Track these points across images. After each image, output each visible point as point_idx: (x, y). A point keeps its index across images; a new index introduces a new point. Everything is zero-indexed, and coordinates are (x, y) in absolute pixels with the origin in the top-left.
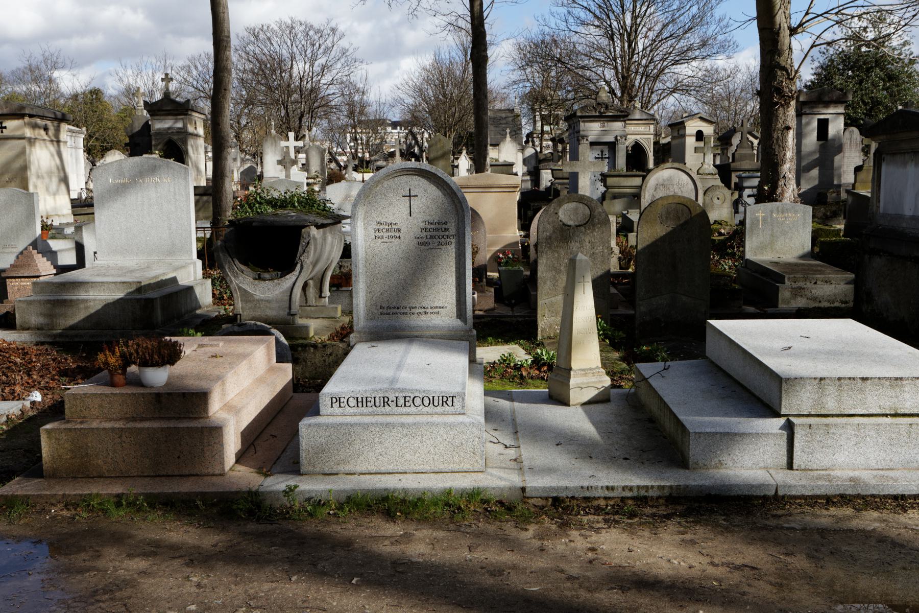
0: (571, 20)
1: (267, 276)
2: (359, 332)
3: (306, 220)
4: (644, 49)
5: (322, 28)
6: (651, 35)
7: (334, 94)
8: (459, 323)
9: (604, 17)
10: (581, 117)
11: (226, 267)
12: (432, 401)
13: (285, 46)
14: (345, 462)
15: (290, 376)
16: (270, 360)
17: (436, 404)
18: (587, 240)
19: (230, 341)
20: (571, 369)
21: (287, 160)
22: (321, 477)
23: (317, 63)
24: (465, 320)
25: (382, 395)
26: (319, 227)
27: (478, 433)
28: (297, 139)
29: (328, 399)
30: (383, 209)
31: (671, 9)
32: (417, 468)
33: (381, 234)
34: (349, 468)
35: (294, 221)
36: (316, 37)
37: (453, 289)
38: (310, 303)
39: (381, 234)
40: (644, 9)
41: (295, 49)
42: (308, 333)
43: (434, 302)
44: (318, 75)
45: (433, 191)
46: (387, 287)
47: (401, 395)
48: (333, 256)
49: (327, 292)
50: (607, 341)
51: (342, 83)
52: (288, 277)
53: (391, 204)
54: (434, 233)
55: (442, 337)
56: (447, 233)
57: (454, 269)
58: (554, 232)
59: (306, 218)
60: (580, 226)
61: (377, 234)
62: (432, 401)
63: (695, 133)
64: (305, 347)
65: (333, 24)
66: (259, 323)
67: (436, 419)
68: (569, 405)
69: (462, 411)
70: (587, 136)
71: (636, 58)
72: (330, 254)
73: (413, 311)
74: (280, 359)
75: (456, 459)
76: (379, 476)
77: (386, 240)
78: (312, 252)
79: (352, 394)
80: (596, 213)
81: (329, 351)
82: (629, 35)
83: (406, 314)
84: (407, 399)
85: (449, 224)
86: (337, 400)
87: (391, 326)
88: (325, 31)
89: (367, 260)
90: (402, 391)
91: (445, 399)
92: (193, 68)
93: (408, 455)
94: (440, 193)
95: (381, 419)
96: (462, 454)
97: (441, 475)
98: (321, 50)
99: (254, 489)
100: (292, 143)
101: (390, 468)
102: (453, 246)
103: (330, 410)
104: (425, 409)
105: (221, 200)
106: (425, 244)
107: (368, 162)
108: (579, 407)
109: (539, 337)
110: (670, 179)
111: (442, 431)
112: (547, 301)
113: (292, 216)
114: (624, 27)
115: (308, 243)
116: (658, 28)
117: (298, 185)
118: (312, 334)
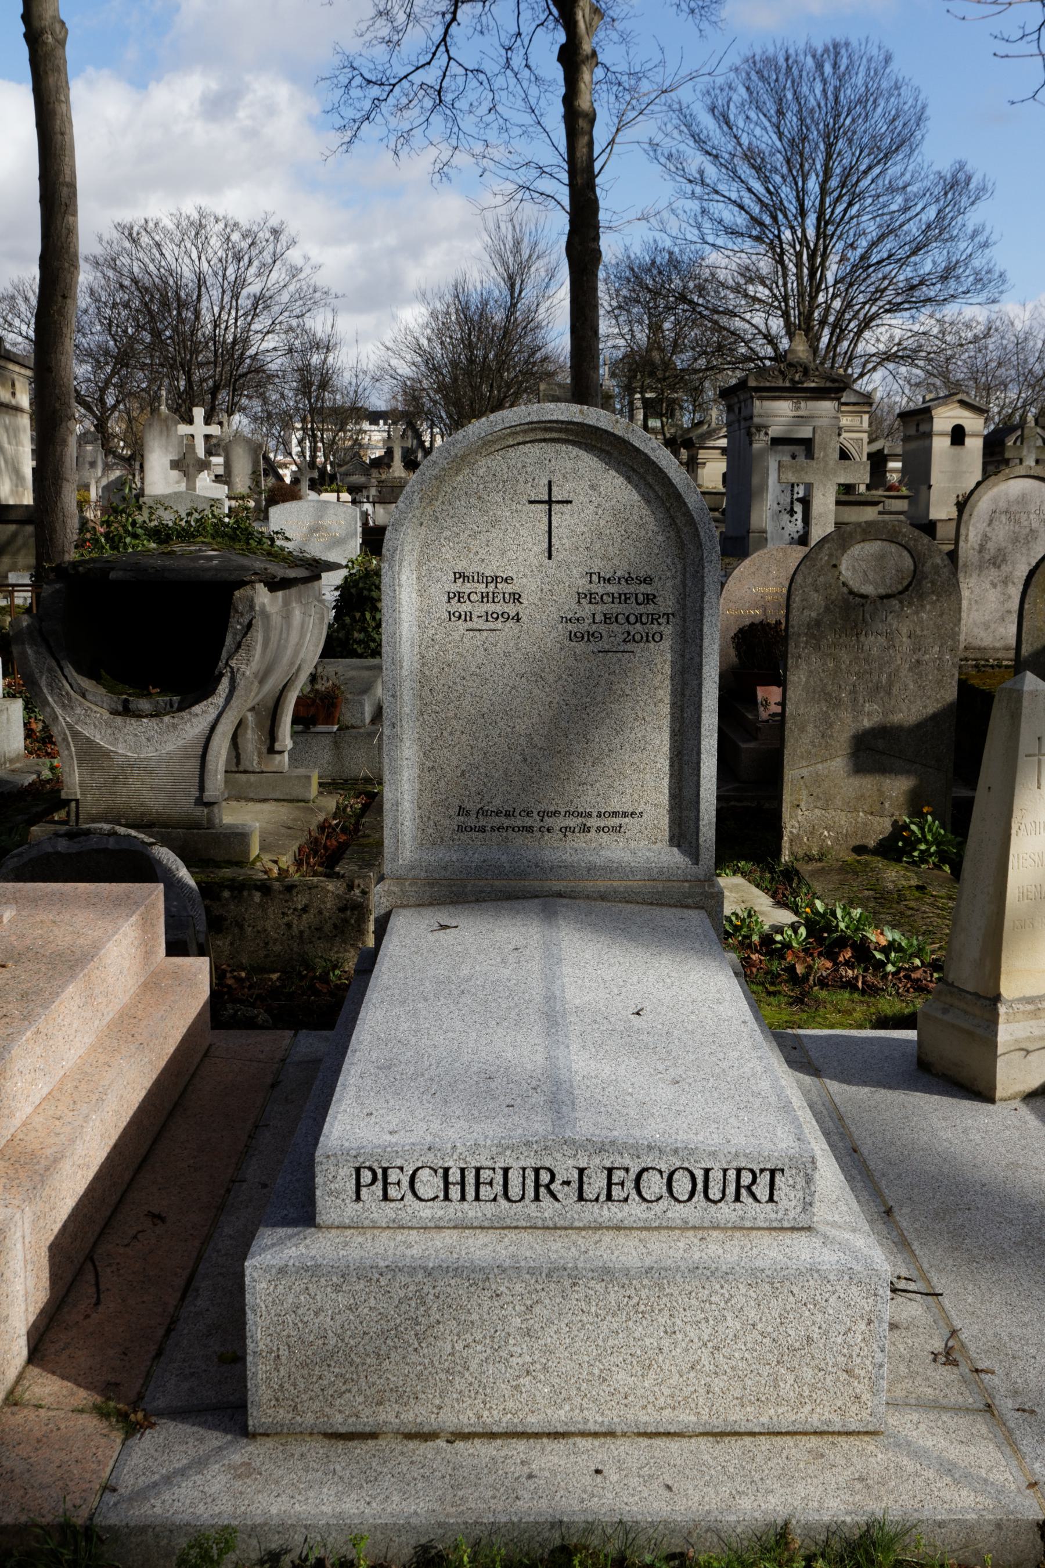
0: (707, 225)
1: (144, 705)
2: (399, 879)
3: (244, 569)
4: (836, 282)
5: (255, 228)
6: (854, 256)
7: (275, 349)
8: (674, 858)
9: (768, 220)
10: (757, 389)
11: (43, 683)
12: (701, 1186)
13: (187, 261)
14: (402, 1398)
15: (204, 992)
16: (148, 954)
17: (715, 1193)
18: (904, 631)
19: (35, 901)
20: (997, 998)
21: (190, 460)
22: (318, 1448)
23: (244, 293)
24: (693, 852)
25: (531, 1162)
26: (275, 585)
27: (867, 1304)
28: (207, 422)
29: (346, 1172)
30: (474, 535)
31: (886, 210)
32: (648, 1419)
33: (466, 607)
34: (418, 1414)
35: (216, 569)
36: (244, 245)
37: (664, 764)
38: (245, 764)
39: (466, 607)
40: (840, 209)
41: (205, 265)
42: (246, 852)
43: (607, 798)
44: (245, 314)
45: (615, 489)
46: (478, 757)
47: (595, 1164)
48: (302, 655)
49: (286, 739)
50: (947, 868)
51: (291, 329)
52: (197, 709)
53: (495, 523)
54: (616, 608)
55: (628, 898)
56: (650, 608)
57: (666, 709)
58: (827, 609)
59: (246, 562)
60: (888, 596)
61: (455, 606)
62: (701, 1186)
63: (949, 429)
64: (240, 888)
65: (274, 222)
66: (122, 830)
67: (718, 1250)
68: (991, 1100)
69: (803, 1221)
70: (767, 427)
71: (821, 298)
72: (296, 653)
73: (549, 821)
74: (175, 948)
76: (521, 1445)
77: (480, 624)
78: (259, 648)
79: (430, 1158)
80: (928, 568)
81: (301, 901)
82: (812, 257)
83: (530, 829)
85: (657, 584)
86: (375, 1176)
87: (505, 868)
88: (261, 235)
89: (423, 680)
90: (601, 1149)
91: (746, 1179)
92: (20, 301)
93: (621, 1377)
94: (636, 497)
95: (529, 1248)
96: (808, 1374)
97: (736, 1445)
98: (253, 270)
99: (79, 1519)
100: (199, 428)
101: (559, 1417)
102: (666, 644)
103: (352, 1209)
104: (678, 1212)
105: (53, 530)
106: (590, 636)
107: (333, 478)
108: (1016, 1103)
109: (786, 857)
110: (1023, 499)
111: (742, 1294)
112: (805, 772)
113: (211, 558)
114: (804, 241)
115: (250, 625)
116: (864, 243)
117: (214, 502)
118: (255, 851)
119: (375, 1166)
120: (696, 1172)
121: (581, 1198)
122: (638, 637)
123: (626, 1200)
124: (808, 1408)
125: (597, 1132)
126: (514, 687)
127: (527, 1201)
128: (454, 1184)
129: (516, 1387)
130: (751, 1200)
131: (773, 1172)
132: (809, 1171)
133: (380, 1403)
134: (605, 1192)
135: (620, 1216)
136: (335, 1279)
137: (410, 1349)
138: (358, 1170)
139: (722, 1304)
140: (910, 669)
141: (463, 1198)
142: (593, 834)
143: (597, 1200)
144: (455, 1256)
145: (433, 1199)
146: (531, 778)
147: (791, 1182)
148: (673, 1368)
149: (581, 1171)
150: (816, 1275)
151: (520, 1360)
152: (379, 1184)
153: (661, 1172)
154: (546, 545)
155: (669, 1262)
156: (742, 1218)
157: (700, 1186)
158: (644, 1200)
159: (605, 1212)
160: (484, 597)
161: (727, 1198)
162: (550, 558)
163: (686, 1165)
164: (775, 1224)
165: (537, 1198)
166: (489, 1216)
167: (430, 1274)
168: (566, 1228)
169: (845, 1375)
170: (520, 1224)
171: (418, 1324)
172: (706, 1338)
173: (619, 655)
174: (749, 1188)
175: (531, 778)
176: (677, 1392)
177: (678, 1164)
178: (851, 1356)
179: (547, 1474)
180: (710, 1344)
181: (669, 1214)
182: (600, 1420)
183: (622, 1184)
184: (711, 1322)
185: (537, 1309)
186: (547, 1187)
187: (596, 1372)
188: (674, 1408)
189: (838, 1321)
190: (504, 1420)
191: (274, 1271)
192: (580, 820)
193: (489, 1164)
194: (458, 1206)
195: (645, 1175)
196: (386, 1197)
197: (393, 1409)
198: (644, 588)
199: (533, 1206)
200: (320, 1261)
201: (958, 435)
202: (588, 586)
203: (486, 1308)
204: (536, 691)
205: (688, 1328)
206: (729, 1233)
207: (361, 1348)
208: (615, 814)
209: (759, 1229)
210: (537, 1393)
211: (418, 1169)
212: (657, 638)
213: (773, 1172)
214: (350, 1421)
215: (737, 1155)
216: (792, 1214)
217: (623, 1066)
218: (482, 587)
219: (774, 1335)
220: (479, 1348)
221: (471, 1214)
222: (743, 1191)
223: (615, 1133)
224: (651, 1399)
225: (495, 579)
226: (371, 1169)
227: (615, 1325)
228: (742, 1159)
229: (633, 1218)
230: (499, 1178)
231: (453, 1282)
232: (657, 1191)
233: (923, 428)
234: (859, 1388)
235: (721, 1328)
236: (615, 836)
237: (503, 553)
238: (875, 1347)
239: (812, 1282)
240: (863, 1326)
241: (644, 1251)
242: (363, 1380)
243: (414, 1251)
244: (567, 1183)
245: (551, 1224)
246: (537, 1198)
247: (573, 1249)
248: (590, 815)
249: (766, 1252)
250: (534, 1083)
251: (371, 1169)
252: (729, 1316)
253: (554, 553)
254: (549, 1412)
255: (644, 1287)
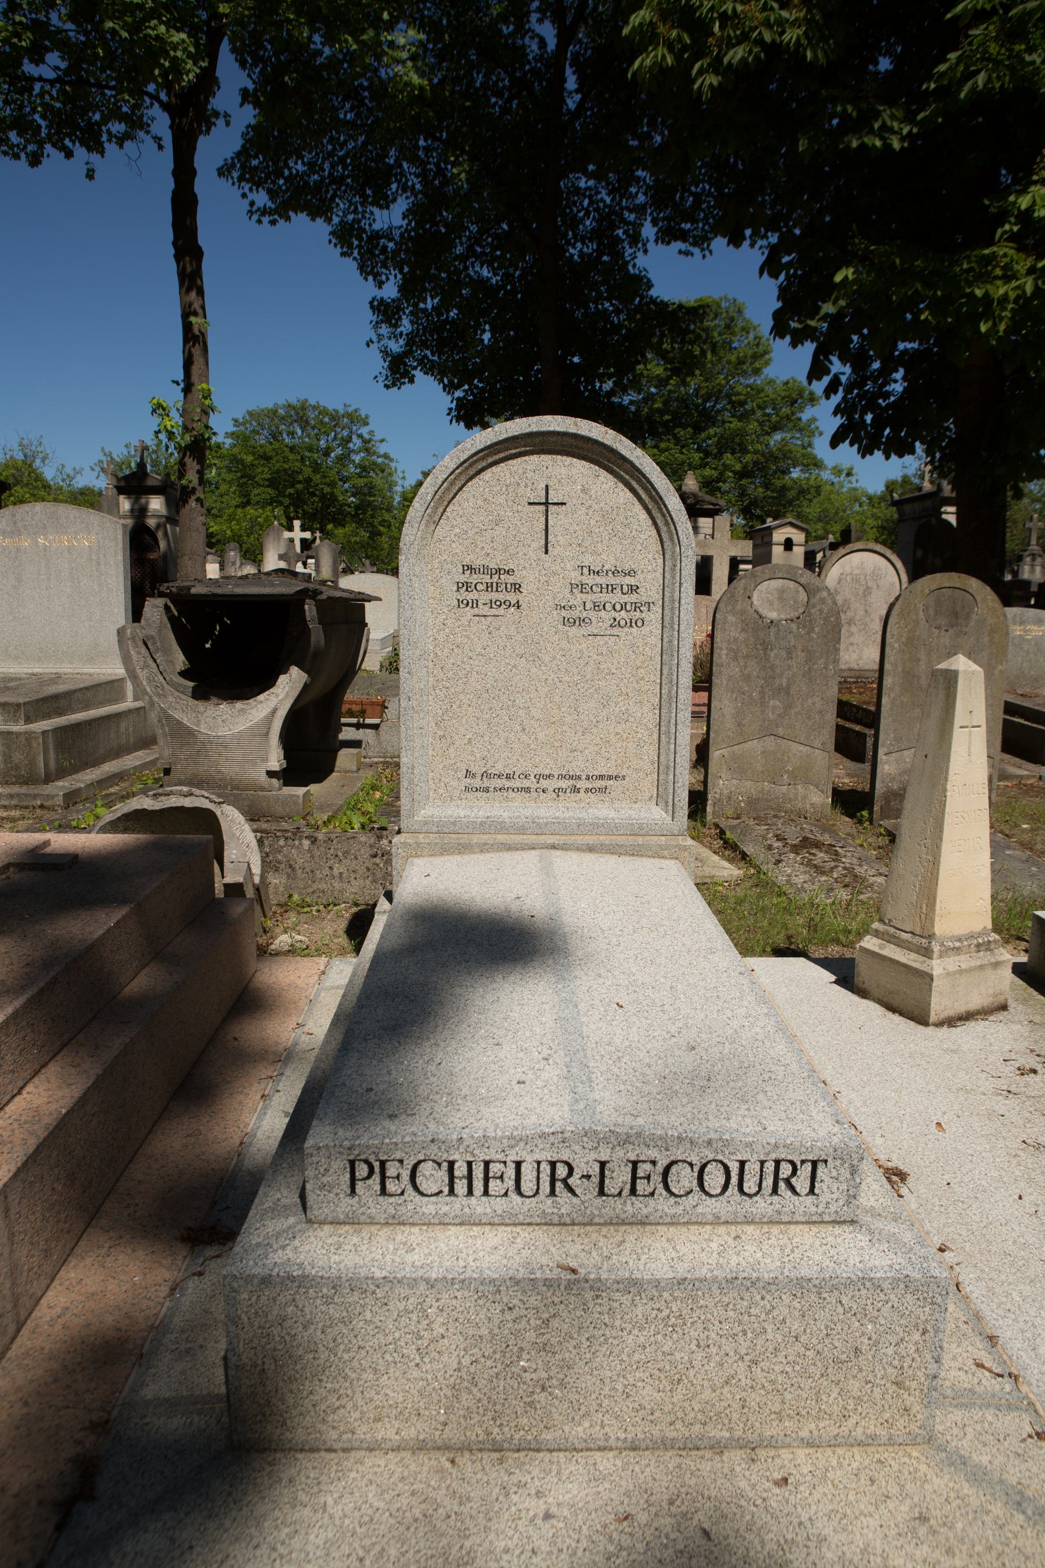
12: (735, 1179)
17: (750, 1186)
28: (303, 529)
39: (471, 596)
56: (634, 598)
61: (464, 595)
69: (846, 1213)
75: (832, 1401)
77: (484, 610)
79: (433, 1151)
84: (643, 1169)
85: (640, 576)
90: (625, 1141)
91: (786, 1170)
96: (854, 1386)
100: (298, 534)
103: (346, 1204)
104: (709, 1207)
119: (372, 1159)
120: (730, 1164)
121: (602, 1192)
122: (622, 623)
123: (652, 1194)
124: (851, 1422)
125: (620, 1120)
126: (515, 666)
127: (542, 1196)
128: (461, 1179)
129: (531, 1404)
130: (789, 1193)
131: (814, 1164)
132: (855, 1162)
133: (377, 1420)
134: (628, 1186)
135: (645, 1211)
136: (325, 1291)
137: (412, 1364)
138: (352, 1163)
139: (763, 1316)
140: (804, 675)
141: (470, 1192)
142: (582, 794)
143: (620, 1194)
144: (462, 1263)
145: (437, 1194)
146: (529, 745)
147: (834, 1173)
148: (706, 1383)
149: (603, 1165)
150: (868, 1284)
151: (533, 1376)
152: (377, 1177)
153: (691, 1165)
154: (543, 542)
155: (704, 1271)
156: (779, 1213)
157: (734, 1180)
158: (672, 1194)
159: (629, 1207)
160: (489, 587)
161: (763, 1191)
162: (546, 552)
163: (720, 1157)
164: (814, 1218)
165: (553, 1193)
166: (499, 1212)
167: (432, 1286)
168: (585, 1225)
169: (894, 1387)
170: (533, 1220)
171: (420, 1338)
172: (744, 1351)
173: (606, 638)
174: (787, 1181)
175: (529, 745)
176: (709, 1407)
177: (711, 1157)
178: (902, 1367)
179: (566, 1512)
180: (747, 1358)
181: (700, 1209)
182: (623, 1436)
183: (648, 1178)
184: (750, 1335)
185: (555, 1323)
186: (564, 1181)
187: (620, 1387)
188: (705, 1424)
189: (890, 1331)
190: (517, 1437)
191: (256, 1281)
192: (571, 782)
193: (500, 1157)
194: (465, 1201)
195: (674, 1169)
196: (384, 1191)
197: (393, 1426)
198: (628, 580)
199: (549, 1202)
200: (308, 1270)
201: (788, 545)
202: (580, 578)
203: (496, 1322)
204: (534, 670)
205: (724, 1340)
206: (766, 1228)
207: (355, 1363)
208: (601, 777)
209: (797, 1223)
210: (554, 1410)
211: (420, 1162)
212: (639, 623)
213: (814, 1164)
214: (345, 1437)
215: (776, 1146)
216: (833, 1208)
217: (634, 1029)
218: (487, 578)
219: (819, 1347)
220: (489, 1363)
221: (480, 1210)
222: (782, 1185)
223: (641, 1121)
224: (680, 1414)
225: (498, 571)
226: (367, 1162)
227: (642, 1339)
228: (781, 1150)
229: (659, 1214)
230: (511, 1172)
231: (459, 1294)
232: (687, 1184)
233: (766, 540)
234: (909, 1400)
235: (760, 1341)
236: (601, 796)
237: (506, 548)
238: (928, 1357)
239: (864, 1292)
240: (917, 1336)
241: (674, 1255)
242: (358, 1395)
243: (415, 1257)
244: (588, 1177)
245: (568, 1220)
246: (553, 1193)
247: (594, 1254)
248: (579, 778)
249: (810, 1254)
250: (546, 1052)
251: (367, 1162)
252: (770, 1328)
253: (550, 549)
254: (567, 1428)
255: (675, 1299)
